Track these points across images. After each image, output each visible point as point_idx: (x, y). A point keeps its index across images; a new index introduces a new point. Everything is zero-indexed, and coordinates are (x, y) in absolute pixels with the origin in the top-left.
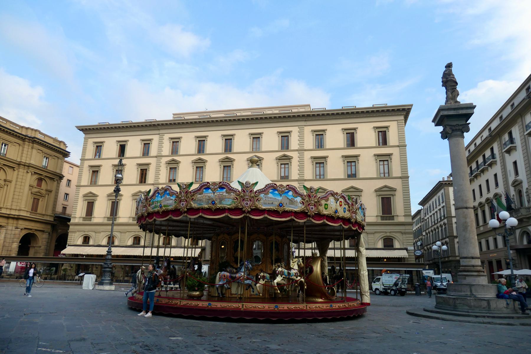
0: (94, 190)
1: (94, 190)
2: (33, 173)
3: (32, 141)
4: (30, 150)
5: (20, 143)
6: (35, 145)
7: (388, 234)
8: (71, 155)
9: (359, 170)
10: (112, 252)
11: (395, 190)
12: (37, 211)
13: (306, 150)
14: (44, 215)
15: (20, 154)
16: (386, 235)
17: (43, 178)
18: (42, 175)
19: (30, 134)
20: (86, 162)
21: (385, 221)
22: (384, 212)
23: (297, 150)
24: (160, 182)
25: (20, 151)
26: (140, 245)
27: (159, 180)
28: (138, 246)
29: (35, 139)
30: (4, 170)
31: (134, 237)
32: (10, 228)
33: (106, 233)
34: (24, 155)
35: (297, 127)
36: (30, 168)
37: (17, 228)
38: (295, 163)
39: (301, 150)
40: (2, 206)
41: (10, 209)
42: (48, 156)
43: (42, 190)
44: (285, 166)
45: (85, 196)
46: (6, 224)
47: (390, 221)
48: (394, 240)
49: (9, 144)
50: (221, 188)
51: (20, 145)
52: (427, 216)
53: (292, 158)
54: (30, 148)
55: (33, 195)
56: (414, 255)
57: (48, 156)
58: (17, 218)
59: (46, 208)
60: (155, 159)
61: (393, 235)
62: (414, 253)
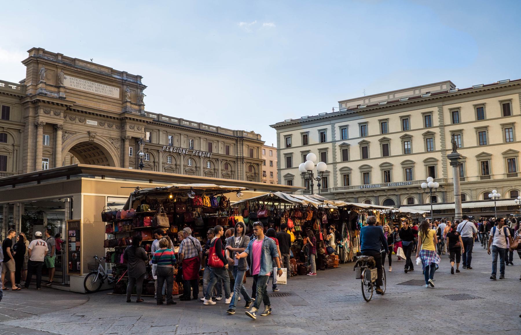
4: (241, 165)
7: (513, 188)
11: (329, 172)
13: (445, 126)
15: (236, 149)
16: (511, 188)
20: (446, 128)
21: (483, 180)
23: (331, 142)
31: (511, 192)
33: (507, 188)
35: (437, 107)
39: (334, 142)
44: (407, 143)
45: (285, 176)
47: (515, 177)
48: (466, 195)
53: (435, 133)
60: (331, 144)
61: (465, 192)
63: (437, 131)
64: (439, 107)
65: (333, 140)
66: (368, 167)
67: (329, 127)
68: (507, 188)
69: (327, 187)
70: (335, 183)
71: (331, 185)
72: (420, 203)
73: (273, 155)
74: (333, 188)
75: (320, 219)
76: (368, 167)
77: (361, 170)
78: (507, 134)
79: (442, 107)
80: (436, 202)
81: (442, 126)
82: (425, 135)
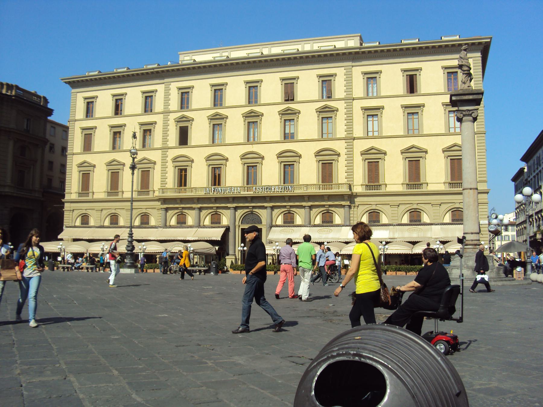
0: (183, 151)
1: (89, 158)
8: (54, 113)
9: (422, 124)
10: (133, 234)
11: (155, 163)
22: (453, 177)
24: (169, 146)
26: (187, 224)
27: (168, 143)
28: (147, 226)
38: (340, 119)
39: (166, 112)
50: (235, 399)
52: (531, 177)
56: (488, 230)
62: (488, 228)
63: (340, 106)
64: (347, 68)
65: (167, 110)
66: (187, 159)
71: (156, 183)
74: (159, 189)
76: (187, 159)
77: (174, 163)
78: (370, 123)
79: (76, 95)
80: (117, 224)
81: (350, 99)
82: (320, 111)
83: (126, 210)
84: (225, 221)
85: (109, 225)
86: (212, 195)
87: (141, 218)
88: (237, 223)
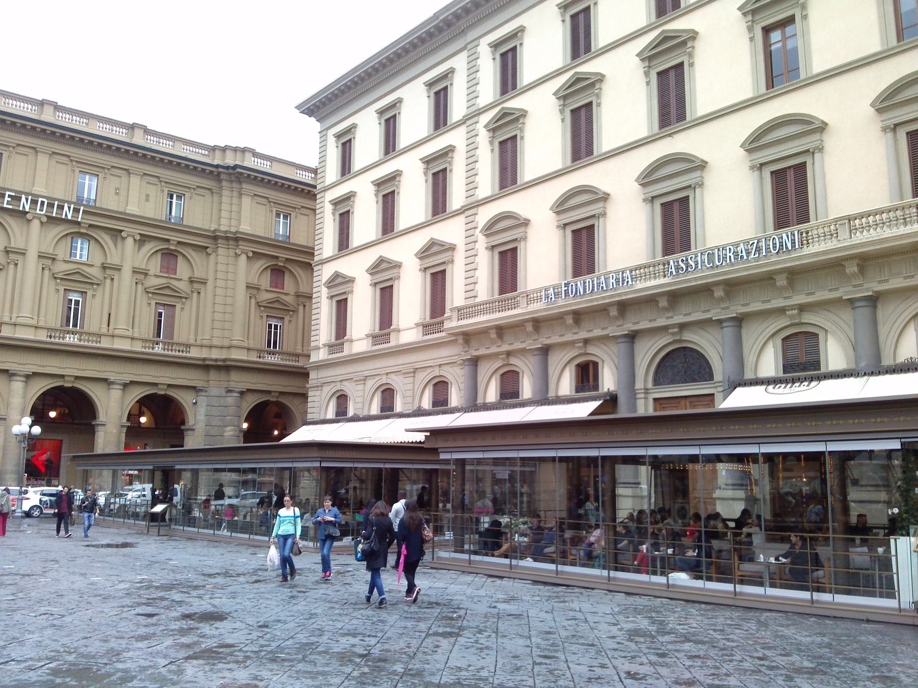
2: (251, 254)
3: (237, 177)
4: (235, 201)
5: (34, 146)
6: (244, 186)
11: (452, 248)
12: (172, 338)
14: (298, 355)
15: (215, 211)
17: (174, 248)
18: (277, 257)
19: (230, 160)
25: (215, 205)
29: (239, 170)
30: (184, 256)
32: (214, 391)
33: (426, 373)
34: (224, 214)
36: (240, 243)
37: (230, 391)
40: (6, 319)
41: (228, 348)
42: (287, 210)
43: (287, 294)
46: (205, 385)
49: (186, 194)
51: (212, 193)
54: (235, 194)
55: (150, 295)
57: (287, 210)
58: (225, 367)
59: (4, 304)
67: (460, 63)
68: (330, 387)
69: (390, 323)
70: (471, 283)
71: (456, 296)
72: (857, 360)
73: (258, 205)
75: (795, 494)
77: (563, 216)
83: (356, 381)
84: (608, 381)
85: (573, 393)
86: (775, 261)
87: (337, 402)
88: (639, 385)
